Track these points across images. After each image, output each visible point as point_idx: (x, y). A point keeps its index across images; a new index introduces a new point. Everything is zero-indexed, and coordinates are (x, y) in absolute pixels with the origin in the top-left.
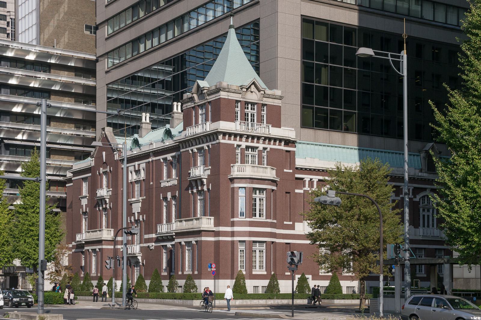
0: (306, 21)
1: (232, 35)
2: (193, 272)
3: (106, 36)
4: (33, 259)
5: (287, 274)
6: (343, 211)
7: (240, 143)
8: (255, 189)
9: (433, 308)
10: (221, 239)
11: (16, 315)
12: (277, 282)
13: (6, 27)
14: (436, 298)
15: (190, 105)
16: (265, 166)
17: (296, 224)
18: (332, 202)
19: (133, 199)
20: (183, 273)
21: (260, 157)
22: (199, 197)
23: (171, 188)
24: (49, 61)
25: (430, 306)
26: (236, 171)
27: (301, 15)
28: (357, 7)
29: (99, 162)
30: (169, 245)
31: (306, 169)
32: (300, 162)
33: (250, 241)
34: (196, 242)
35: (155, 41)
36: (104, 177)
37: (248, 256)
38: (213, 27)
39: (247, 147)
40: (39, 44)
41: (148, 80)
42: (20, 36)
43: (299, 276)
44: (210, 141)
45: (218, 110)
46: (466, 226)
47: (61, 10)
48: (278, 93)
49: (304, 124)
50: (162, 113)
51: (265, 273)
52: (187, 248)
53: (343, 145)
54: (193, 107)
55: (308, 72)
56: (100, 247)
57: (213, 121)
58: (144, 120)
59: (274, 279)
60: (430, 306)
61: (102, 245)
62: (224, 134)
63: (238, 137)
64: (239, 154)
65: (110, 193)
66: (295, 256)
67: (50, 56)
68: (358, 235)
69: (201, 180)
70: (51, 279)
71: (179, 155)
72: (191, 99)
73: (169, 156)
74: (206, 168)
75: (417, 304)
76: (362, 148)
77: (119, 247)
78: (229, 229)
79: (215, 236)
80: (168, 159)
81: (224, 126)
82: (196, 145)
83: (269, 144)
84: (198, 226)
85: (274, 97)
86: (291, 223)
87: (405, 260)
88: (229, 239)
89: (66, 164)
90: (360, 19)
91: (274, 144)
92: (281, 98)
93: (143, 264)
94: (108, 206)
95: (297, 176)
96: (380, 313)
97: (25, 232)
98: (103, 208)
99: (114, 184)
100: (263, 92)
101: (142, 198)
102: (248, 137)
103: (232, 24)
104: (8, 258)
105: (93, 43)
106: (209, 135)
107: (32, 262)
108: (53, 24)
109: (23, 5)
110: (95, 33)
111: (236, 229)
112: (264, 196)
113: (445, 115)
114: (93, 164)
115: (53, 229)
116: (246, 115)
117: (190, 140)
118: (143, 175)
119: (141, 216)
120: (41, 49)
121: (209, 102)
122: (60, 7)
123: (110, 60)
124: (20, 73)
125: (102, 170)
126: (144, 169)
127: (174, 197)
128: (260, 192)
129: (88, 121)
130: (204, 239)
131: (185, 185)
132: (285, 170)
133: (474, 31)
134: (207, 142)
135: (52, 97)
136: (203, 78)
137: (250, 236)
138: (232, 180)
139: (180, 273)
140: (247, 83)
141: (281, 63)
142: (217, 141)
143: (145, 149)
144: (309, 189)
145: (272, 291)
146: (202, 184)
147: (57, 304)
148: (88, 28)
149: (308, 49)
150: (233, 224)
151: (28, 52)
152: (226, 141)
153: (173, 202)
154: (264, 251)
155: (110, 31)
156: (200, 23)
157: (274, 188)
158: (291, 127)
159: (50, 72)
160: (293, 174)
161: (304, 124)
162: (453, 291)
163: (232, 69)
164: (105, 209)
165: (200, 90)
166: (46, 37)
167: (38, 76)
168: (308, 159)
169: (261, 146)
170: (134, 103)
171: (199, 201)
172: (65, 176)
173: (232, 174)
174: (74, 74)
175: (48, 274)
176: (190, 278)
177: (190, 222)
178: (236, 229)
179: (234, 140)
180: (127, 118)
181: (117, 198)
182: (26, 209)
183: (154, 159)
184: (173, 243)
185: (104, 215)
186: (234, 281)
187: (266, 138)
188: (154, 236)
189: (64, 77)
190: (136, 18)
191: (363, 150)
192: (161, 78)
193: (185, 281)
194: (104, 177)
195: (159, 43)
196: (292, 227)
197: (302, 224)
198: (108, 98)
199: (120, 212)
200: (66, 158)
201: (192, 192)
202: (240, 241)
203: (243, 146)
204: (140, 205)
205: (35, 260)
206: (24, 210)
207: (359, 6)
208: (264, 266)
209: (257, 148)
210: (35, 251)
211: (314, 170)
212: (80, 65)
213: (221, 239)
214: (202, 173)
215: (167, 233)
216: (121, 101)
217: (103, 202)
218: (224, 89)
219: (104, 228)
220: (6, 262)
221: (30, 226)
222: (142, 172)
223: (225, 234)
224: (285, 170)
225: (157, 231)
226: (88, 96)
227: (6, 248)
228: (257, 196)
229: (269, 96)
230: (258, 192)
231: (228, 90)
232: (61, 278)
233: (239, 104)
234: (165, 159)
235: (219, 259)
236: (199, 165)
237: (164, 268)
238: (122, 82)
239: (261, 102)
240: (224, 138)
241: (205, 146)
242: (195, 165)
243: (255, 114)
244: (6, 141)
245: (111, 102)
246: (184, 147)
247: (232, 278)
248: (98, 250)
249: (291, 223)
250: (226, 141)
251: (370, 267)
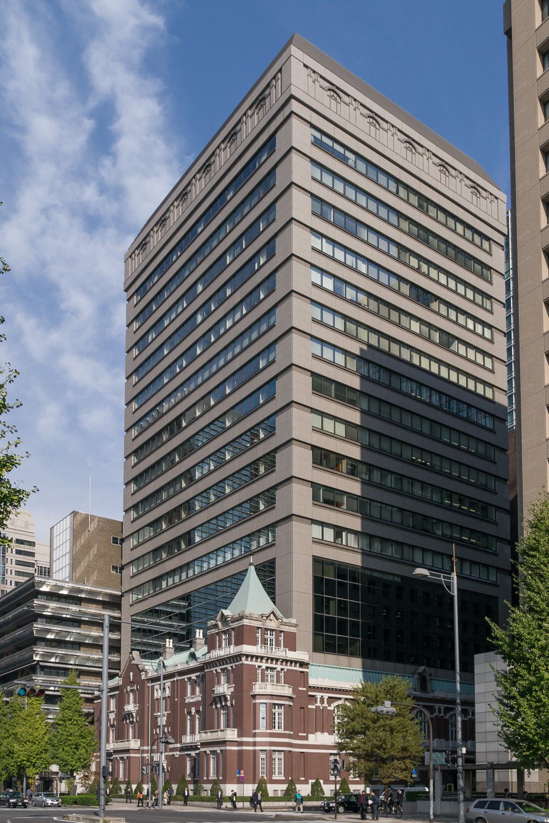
0: (317, 560)
1: (252, 570)
2: (218, 778)
3: (131, 575)
4: (71, 766)
5: (301, 779)
6: (371, 723)
7: (260, 664)
8: (275, 704)
9: (500, 812)
10: (244, 748)
11: (77, 818)
12: (295, 787)
13: (34, 572)
14: (504, 802)
15: (214, 631)
16: (283, 684)
17: (309, 735)
18: (388, 712)
19: (159, 714)
20: (208, 777)
21: (278, 675)
22: (222, 712)
23: (195, 704)
24: (80, 596)
25: (498, 809)
26: (258, 688)
27: (313, 556)
28: (360, 551)
29: (126, 681)
30: (193, 753)
31: (318, 688)
32: (312, 682)
33: (270, 750)
34: (127, 757)
35: (177, 579)
36: (131, 694)
37: (268, 763)
38: (232, 566)
39: (267, 668)
40: (71, 580)
41: (168, 613)
42: (54, 575)
43: (314, 781)
44: (234, 662)
45: (241, 635)
46: (532, 733)
47: (91, 553)
48: (294, 621)
49: (316, 649)
50: (184, 640)
51: (284, 778)
52: (211, 756)
53: (349, 667)
54: (217, 633)
55: (319, 604)
56: (128, 755)
57: (237, 644)
58: (167, 646)
59: (291, 784)
60: (498, 809)
61: (130, 753)
62: (247, 656)
63: (259, 659)
64: (260, 674)
65: (137, 708)
66: (338, 763)
67: (81, 591)
68: (386, 744)
69: (225, 696)
70: (82, 783)
71: (202, 675)
72: (216, 626)
73: (193, 676)
75: (483, 808)
76: (365, 669)
77: (145, 755)
78: (251, 739)
79: (238, 746)
80: (193, 678)
81: (247, 649)
82: (220, 665)
83: (286, 665)
84: (223, 737)
85: (290, 625)
86: (305, 734)
87: (458, 766)
88: (251, 748)
89: (93, 683)
90: (363, 561)
91: (291, 666)
92: (296, 626)
93: (168, 770)
94: (229, 704)
95: (310, 693)
96: (430, 815)
97: (64, 741)
98: (130, 722)
99: (140, 700)
100: (280, 620)
101: (167, 712)
102: (268, 658)
104: (45, 764)
105: (119, 581)
106: (233, 657)
107: (70, 768)
108: (84, 564)
109: (58, 549)
110: (121, 572)
111: (258, 739)
112: (282, 711)
113: (505, 629)
114: (121, 683)
115: (89, 739)
116: (266, 640)
117: (224, 658)
118: (168, 693)
119: (166, 728)
120: (73, 585)
121: (232, 629)
122: (91, 550)
123: (134, 596)
124: (54, 605)
125: (129, 688)
127: (197, 712)
128: (278, 707)
129: (115, 647)
130: (228, 748)
131: (209, 701)
132: (300, 689)
133: (532, 553)
134: (231, 663)
135: (82, 626)
136: (226, 609)
137: (270, 746)
138: (254, 696)
139: (205, 778)
140: (267, 612)
141: (295, 596)
142: (241, 662)
143: (170, 670)
144: (320, 705)
145: (290, 794)
146: (226, 700)
147: (94, 805)
148: (115, 568)
149: (318, 583)
150: (255, 735)
151: (62, 588)
152: (249, 662)
153: (197, 716)
154: (283, 759)
155: (135, 571)
156: (211, 566)
157: (291, 704)
158: (304, 651)
159: (80, 605)
160: (307, 691)
161: (316, 649)
162: (496, 794)
163: (252, 600)
164: (132, 722)
165: (224, 619)
166: (78, 575)
167: (71, 608)
168: (320, 679)
169: (279, 667)
170: (157, 632)
171: (222, 715)
172: (93, 694)
173: (253, 691)
174: (101, 606)
175: (80, 779)
176: (215, 783)
177: (215, 734)
178: (258, 739)
180: (150, 645)
181: (143, 712)
182: (64, 721)
183: (179, 678)
184: (197, 752)
185: (131, 728)
186: (256, 785)
187: (283, 660)
188: (179, 745)
189: (93, 609)
190: (159, 559)
191: (366, 672)
192: (177, 611)
194: (131, 694)
195: (180, 580)
196: (306, 738)
197: (314, 735)
198: (132, 628)
199: (146, 725)
200: (93, 679)
201: (216, 707)
202: (261, 750)
203: (264, 667)
204: (165, 718)
205: (73, 767)
206: (62, 722)
207: (361, 549)
208: (283, 772)
209: (275, 668)
210: (72, 758)
211: (325, 688)
212: (107, 599)
213: (244, 748)
214: (226, 690)
215: (191, 743)
216: (144, 630)
217: (130, 716)
218: (247, 617)
219: (130, 738)
220: (44, 768)
221: (68, 736)
223: (248, 744)
224: (300, 689)
225: (181, 741)
226: (115, 626)
227: (44, 756)
228: (276, 710)
229: (286, 624)
230: (277, 707)
231: (250, 618)
232: (91, 783)
233: (260, 630)
234: (189, 679)
235: (242, 765)
236: (222, 683)
237: (188, 774)
238: (143, 614)
239: (279, 629)
240: (247, 660)
241: (229, 667)
242: (219, 683)
243: (274, 640)
244: (41, 663)
245: (135, 631)
246: (209, 667)
247: (254, 783)
248: (125, 758)
249: (305, 734)
250: (249, 662)
251: (395, 773)
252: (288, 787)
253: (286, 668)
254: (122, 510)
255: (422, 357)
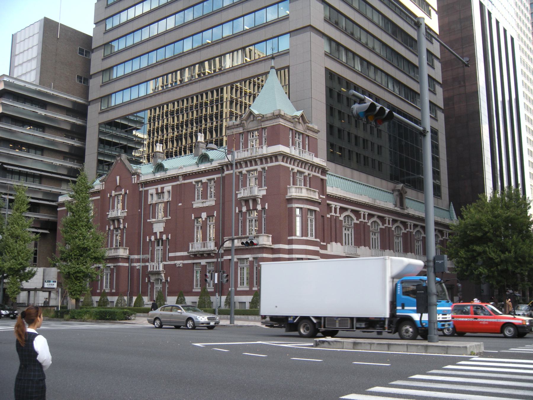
7: (293, 167)
65: (125, 214)
74: (260, 189)
78: (286, 247)
86: (325, 244)
95: (328, 202)
98: (115, 228)
103: (273, 65)
111: (295, 247)
126: (169, 192)
130: (121, 264)
143: (169, 173)
150: (291, 242)
179: (290, 164)
188: (185, 254)
193: (176, 297)
196: (325, 248)
203: (296, 171)
209: (303, 173)
222: (166, 195)
249: (325, 244)
252: (253, 298)
253: (313, 173)
254: (92, 21)
255: (91, 73)
